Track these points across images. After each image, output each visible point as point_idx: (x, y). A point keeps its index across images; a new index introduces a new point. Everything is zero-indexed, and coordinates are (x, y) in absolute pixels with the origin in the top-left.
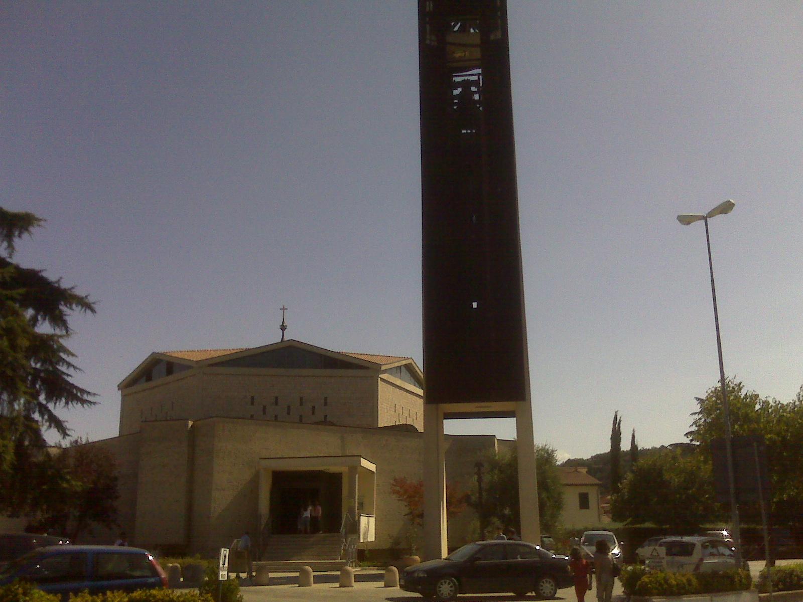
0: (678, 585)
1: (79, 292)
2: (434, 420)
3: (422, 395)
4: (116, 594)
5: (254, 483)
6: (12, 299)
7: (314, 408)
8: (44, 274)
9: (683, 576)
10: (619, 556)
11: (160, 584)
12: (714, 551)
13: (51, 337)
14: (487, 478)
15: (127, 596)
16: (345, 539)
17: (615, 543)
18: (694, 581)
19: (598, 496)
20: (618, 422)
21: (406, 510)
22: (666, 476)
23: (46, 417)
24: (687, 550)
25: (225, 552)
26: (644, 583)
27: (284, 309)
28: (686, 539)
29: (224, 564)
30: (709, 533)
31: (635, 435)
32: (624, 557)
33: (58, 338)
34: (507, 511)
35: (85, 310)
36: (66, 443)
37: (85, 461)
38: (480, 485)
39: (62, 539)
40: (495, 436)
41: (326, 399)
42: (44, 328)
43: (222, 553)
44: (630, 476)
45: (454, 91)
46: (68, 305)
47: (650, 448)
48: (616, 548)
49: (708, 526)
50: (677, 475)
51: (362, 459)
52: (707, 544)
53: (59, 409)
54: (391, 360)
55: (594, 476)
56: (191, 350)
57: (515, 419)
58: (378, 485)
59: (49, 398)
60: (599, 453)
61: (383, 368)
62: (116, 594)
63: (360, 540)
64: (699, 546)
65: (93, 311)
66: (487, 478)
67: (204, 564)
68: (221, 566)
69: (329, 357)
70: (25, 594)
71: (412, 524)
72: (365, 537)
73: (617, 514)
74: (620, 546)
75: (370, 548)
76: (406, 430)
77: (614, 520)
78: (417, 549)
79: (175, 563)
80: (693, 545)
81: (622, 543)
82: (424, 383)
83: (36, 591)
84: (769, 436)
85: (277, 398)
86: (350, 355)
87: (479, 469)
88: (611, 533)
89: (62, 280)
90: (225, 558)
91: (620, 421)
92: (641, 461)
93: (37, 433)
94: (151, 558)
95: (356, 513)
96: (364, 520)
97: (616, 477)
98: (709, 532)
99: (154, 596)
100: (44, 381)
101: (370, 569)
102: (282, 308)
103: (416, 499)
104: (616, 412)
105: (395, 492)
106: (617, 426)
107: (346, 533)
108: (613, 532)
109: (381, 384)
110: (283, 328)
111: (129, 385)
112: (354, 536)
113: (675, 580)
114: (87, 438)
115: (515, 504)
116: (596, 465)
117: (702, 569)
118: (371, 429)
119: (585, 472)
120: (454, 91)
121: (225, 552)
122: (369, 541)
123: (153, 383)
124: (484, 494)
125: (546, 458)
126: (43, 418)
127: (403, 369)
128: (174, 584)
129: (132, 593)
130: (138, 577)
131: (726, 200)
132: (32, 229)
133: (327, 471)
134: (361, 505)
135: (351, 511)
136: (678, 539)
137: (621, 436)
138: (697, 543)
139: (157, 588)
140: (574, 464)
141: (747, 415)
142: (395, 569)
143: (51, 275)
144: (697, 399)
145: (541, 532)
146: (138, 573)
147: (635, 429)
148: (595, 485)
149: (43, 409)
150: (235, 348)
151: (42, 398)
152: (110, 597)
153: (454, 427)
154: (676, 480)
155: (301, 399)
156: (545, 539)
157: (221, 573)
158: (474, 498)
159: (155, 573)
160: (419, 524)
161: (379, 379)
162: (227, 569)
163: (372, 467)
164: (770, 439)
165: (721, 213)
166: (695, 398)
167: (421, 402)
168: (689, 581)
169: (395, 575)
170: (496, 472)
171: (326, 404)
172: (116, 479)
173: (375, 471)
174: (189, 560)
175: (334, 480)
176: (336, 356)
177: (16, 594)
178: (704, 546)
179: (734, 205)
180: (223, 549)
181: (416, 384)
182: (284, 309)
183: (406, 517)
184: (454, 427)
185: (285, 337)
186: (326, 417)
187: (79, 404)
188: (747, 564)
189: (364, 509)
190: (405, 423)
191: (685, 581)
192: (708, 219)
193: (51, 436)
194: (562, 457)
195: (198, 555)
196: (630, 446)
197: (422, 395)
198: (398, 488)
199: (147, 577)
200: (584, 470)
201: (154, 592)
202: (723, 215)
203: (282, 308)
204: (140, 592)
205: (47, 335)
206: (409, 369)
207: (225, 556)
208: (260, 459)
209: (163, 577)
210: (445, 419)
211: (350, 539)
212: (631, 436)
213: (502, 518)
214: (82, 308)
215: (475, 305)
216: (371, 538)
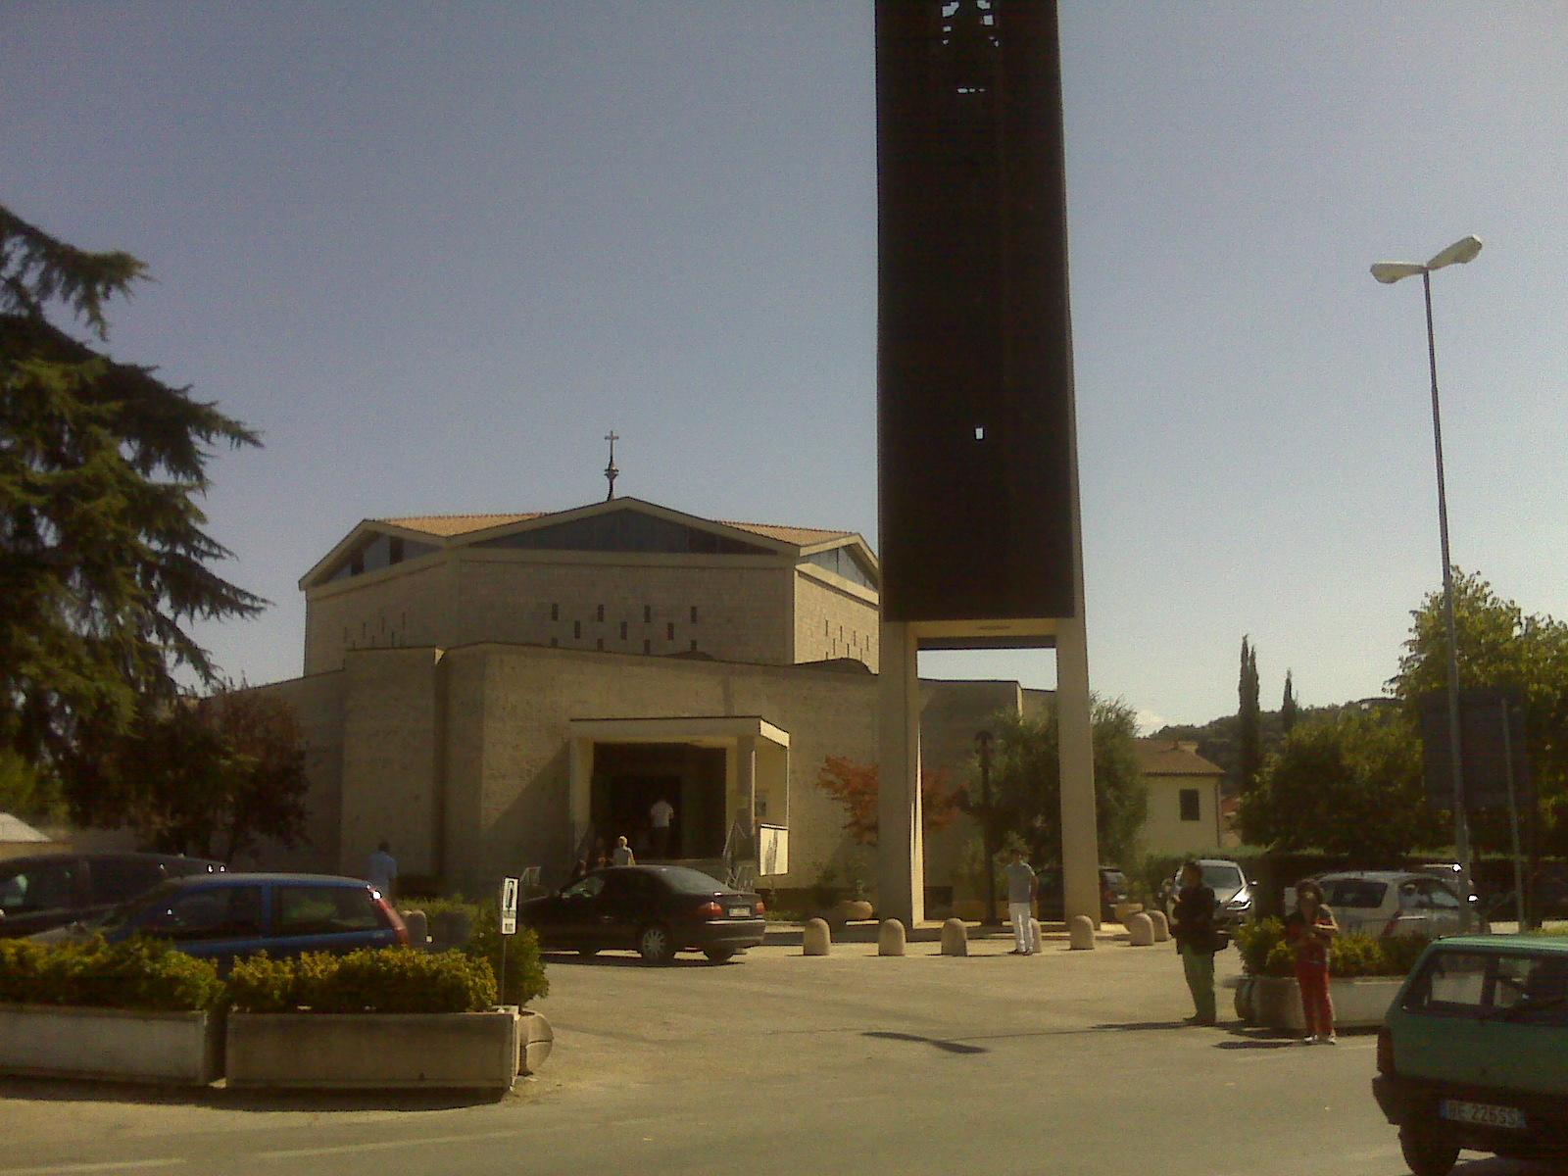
0: (1344, 957)
1: (227, 410)
2: (899, 651)
3: (877, 602)
4: (317, 957)
5: (561, 764)
6: (102, 422)
7: (671, 626)
8: (155, 376)
9: (1356, 941)
10: (1247, 906)
11: (395, 941)
12: (1425, 898)
13: (171, 491)
14: (1000, 761)
15: (336, 961)
16: (733, 869)
17: (1241, 882)
18: (1377, 952)
19: (1217, 798)
20: (1249, 654)
21: (848, 818)
22: (1347, 760)
23: (171, 642)
24: (1371, 896)
25: (510, 885)
26: (1281, 954)
27: (612, 438)
28: (1370, 876)
29: (510, 906)
30: (1427, 868)
31: (1293, 680)
32: (1256, 907)
33: (184, 491)
34: (1040, 821)
35: (239, 444)
36: (203, 691)
37: (243, 722)
38: (985, 772)
39: (212, 862)
40: (1016, 682)
41: (694, 609)
42: (160, 475)
43: (506, 887)
44: (1274, 758)
45: (944, 8)
46: (204, 434)
47: (1326, 706)
48: (1244, 890)
49: (1425, 855)
50: (1368, 758)
51: (762, 722)
52: (1413, 886)
53: (199, 627)
54: (818, 537)
55: (1213, 759)
56: (437, 515)
57: (1055, 650)
58: (793, 772)
59: (178, 604)
60: (1225, 715)
61: (803, 552)
62: (317, 957)
63: (759, 870)
64: (1394, 888)
65: (255, 443)
66: (1000, 761)
67: (471, 910)
68: (505, 909)
69: (700, 532)
70: (154, 957)
71: (857, 844)
72: (770, 865)
73: (1252, 827)
74: (1250, 887)
75: (779, 886)
76: (845, 669)
77: (1246, 841)
78: (866, 890)
79: (418, 910)
80: (1384, 887)
81: (1254, 883)
82: (879, 576)
83: (173, 952)
84: (1536, 687)
85: (601, 608)
86: (744, 527)
87: (984, 743)
88: (1234, 865)
89: (191, 390)
90: (511, 900)
91: (1253, 654)
92: (1301, 732)
93: (160, 671)
94: (377, 895)
95: (753, 822)
96: (766, 835)
97: (1251, 759)
98: (1427, 866)
99: (386, 961)
100: (165, 573)
101: (780, 925)
102: (608, 434)
103: (867, 798)
104: (1245, 638)
105: (829, 784)
106: (1249, 664)
107: (733, 859)
108: (1239, 864)
109: (800, 586)
110: (611, 474)
111: (317, 582)
112: (750, 865)
113: (1341, 950)
114: (175, 665)
115: (1052, 809)
116: (1209, 740)
117: (1399, 931)
118: (780, 667)
119: (1193, 751)
120: (944, 8)
121: (510, 885)
122: (777, 872)
123: (364, 578)
124: (994, 789)
125: (1118, 726)
126: (165, 642)
127: (842, 552)
128: (414, 939)
129: (347, 954)
130: (357, 929)
131: (1465, 236)
132: (130, 284)
133: (696, 744)
134: (762, 807)
135: (743, 816)
136: (1353, 875)
137: (1259, 682)
138: (1391, 883)
139: (391, 946)
140: (1172, 736)
141: (1493, 646)
142: (823, 923)
143: (169, 377)
144: (1414, 612)
145: (1101, 861)
146: (354, 923)
147: (1293, 672)
148: (1213, 775)
149: (166, 628)
150: (521, 512)
151: (164, 606)
152: (306, 963)
153: (937, 665)
154: (1367, 767)
155: (647, 609)
156: (1109, 875)
157: (505, 921)
158: (975, 799)
159: (385, 923)
160: (870, 843)
161: (796, 573)
162: (515, 914)
163: (782, 738)
164: (1538, 694)
165: (1456, 260)
166: (1411, 612)
167: (874, 616)
168: (1367, 952)
169: (823, 934)
170: (1020, 749)
171: (694, 618)
172: (302, 755)
173: (787, 745)
174: (441, 905)
175: (711, 762)
176: (712, 529)
177: (139, 958)
178: (1404, 891)
179: (1479, 246)
180: (507, 880)
181: (868, 582)
182: (612, 438)
183: (847, 830)
184: (937, 665)
185: (614, 492)
186: (694, 643)
187: (236, 615)
188: (1489, 926)
189: (766, 814)
190: (845, 656)
191: (1358, 951)
192: (1430, 272)
193: (185, 677)
194: (1148, 723)
195: (458, 896)
196: (1282, 703)
197: (877, 602)
198: (831, 777)
199: (369, 929)
200: (1191, 748)
201: (386, 953)
202: (1459, 265)
203: (608, 434)
204: (361, 953)
205: (165, 486)
206: (854, 552)
207: (512, 891)
208: (572, 720)
209: (399, 928)
210: (921, 649)
211: (740, 868)
212: (1285, 684)
213: (1031, 835)
214: (233, 438)
215: (979, 433)
216: (781, 867)
